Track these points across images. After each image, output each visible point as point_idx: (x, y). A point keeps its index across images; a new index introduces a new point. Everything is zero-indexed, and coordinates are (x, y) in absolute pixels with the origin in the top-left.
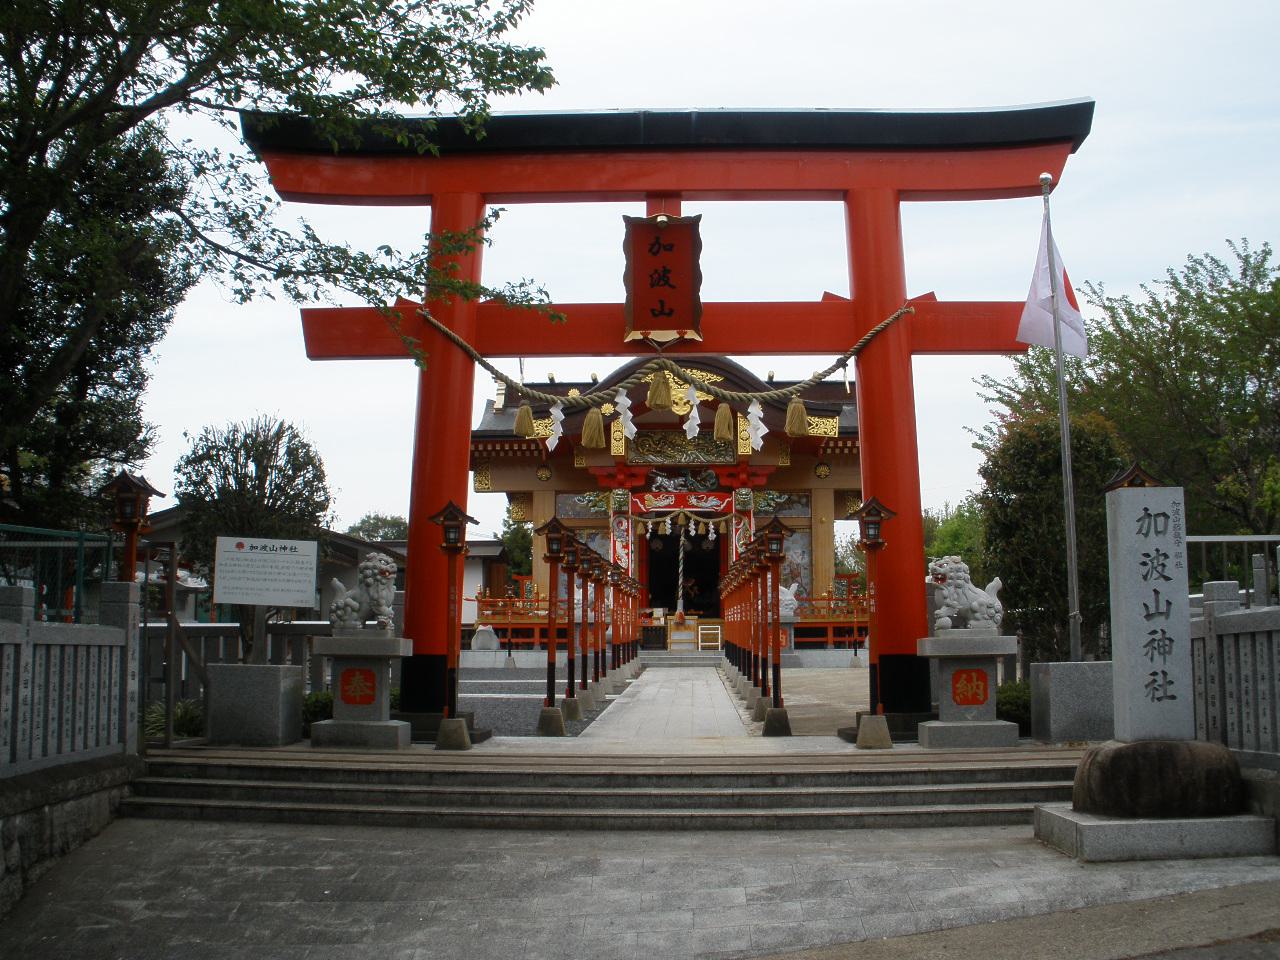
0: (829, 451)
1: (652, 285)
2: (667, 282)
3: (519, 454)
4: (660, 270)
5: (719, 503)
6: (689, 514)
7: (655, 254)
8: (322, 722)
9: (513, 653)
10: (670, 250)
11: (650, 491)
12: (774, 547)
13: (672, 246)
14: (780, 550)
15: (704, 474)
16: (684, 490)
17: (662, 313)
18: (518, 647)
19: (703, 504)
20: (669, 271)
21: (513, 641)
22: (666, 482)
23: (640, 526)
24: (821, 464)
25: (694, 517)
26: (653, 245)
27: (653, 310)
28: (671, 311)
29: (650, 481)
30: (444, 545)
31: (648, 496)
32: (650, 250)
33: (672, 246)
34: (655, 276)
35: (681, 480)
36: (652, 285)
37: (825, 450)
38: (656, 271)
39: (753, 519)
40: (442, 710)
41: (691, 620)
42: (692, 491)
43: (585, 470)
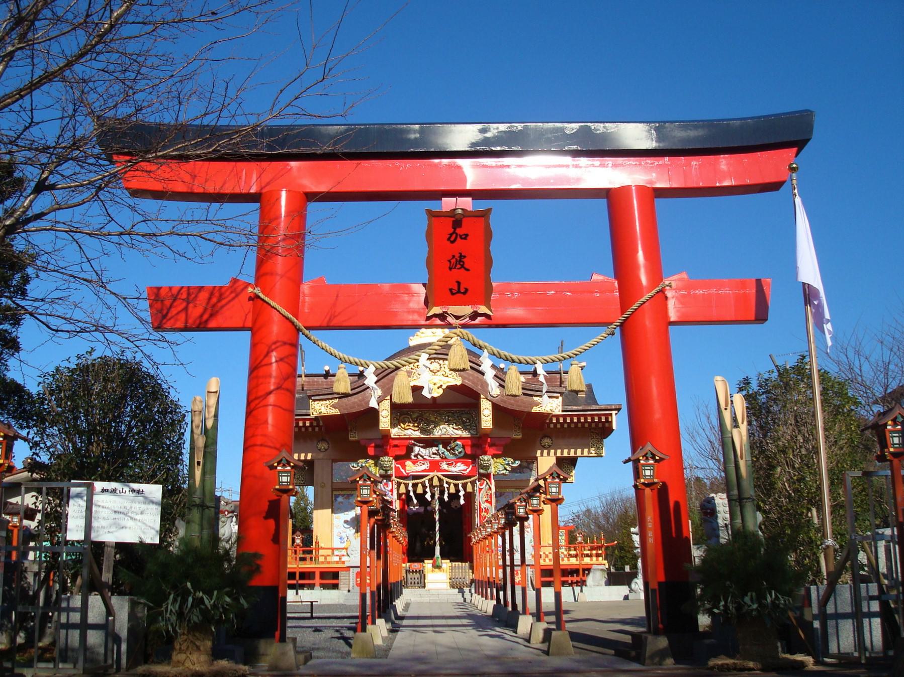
0: (552, 426)
1: (450, 269)
2: (462, 266)
3: (303, 429)
4: (457, 256)
5: (465, 468)
6: (442, 477)
7: (452, 242)
8: (803, 636)
9: (300, 591)
10: (465, 238)
11: (410, 459)
12: (554, 490)
13: (467, 235)
14: (559, 493)
15: (453, 445)
16: (437, 458)
17: (459, 292)
18: (302, 587)
19: (452, 469)
20: (465, 257)
21: (300, 582)
22: (423, 451)
23: (402, 486)
24: (545, 436)
25: (445, 479)
26: (451, 235)
27: (451, 290)
28: (466, 290)
29: (410, 450)
30: (277, 487)
31: (408, 463)
32: (449, 239)
33: (467, 235)
34: (453, 261)
35: (434, 449)
36: (450, 269)
37: (548, 426)
38: (454, 256)
39: (493, 481)
40: (273, 636)
41: (446, 564)
42: (444, 458)
43: (358, 442)
